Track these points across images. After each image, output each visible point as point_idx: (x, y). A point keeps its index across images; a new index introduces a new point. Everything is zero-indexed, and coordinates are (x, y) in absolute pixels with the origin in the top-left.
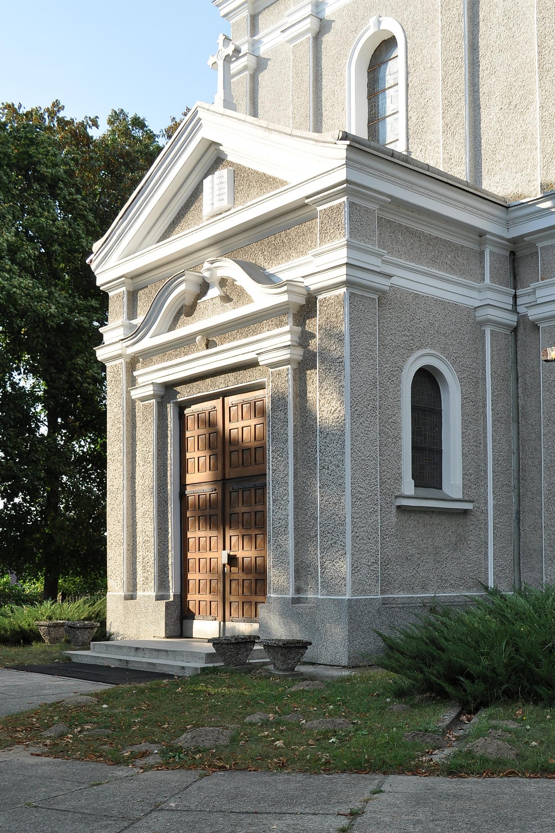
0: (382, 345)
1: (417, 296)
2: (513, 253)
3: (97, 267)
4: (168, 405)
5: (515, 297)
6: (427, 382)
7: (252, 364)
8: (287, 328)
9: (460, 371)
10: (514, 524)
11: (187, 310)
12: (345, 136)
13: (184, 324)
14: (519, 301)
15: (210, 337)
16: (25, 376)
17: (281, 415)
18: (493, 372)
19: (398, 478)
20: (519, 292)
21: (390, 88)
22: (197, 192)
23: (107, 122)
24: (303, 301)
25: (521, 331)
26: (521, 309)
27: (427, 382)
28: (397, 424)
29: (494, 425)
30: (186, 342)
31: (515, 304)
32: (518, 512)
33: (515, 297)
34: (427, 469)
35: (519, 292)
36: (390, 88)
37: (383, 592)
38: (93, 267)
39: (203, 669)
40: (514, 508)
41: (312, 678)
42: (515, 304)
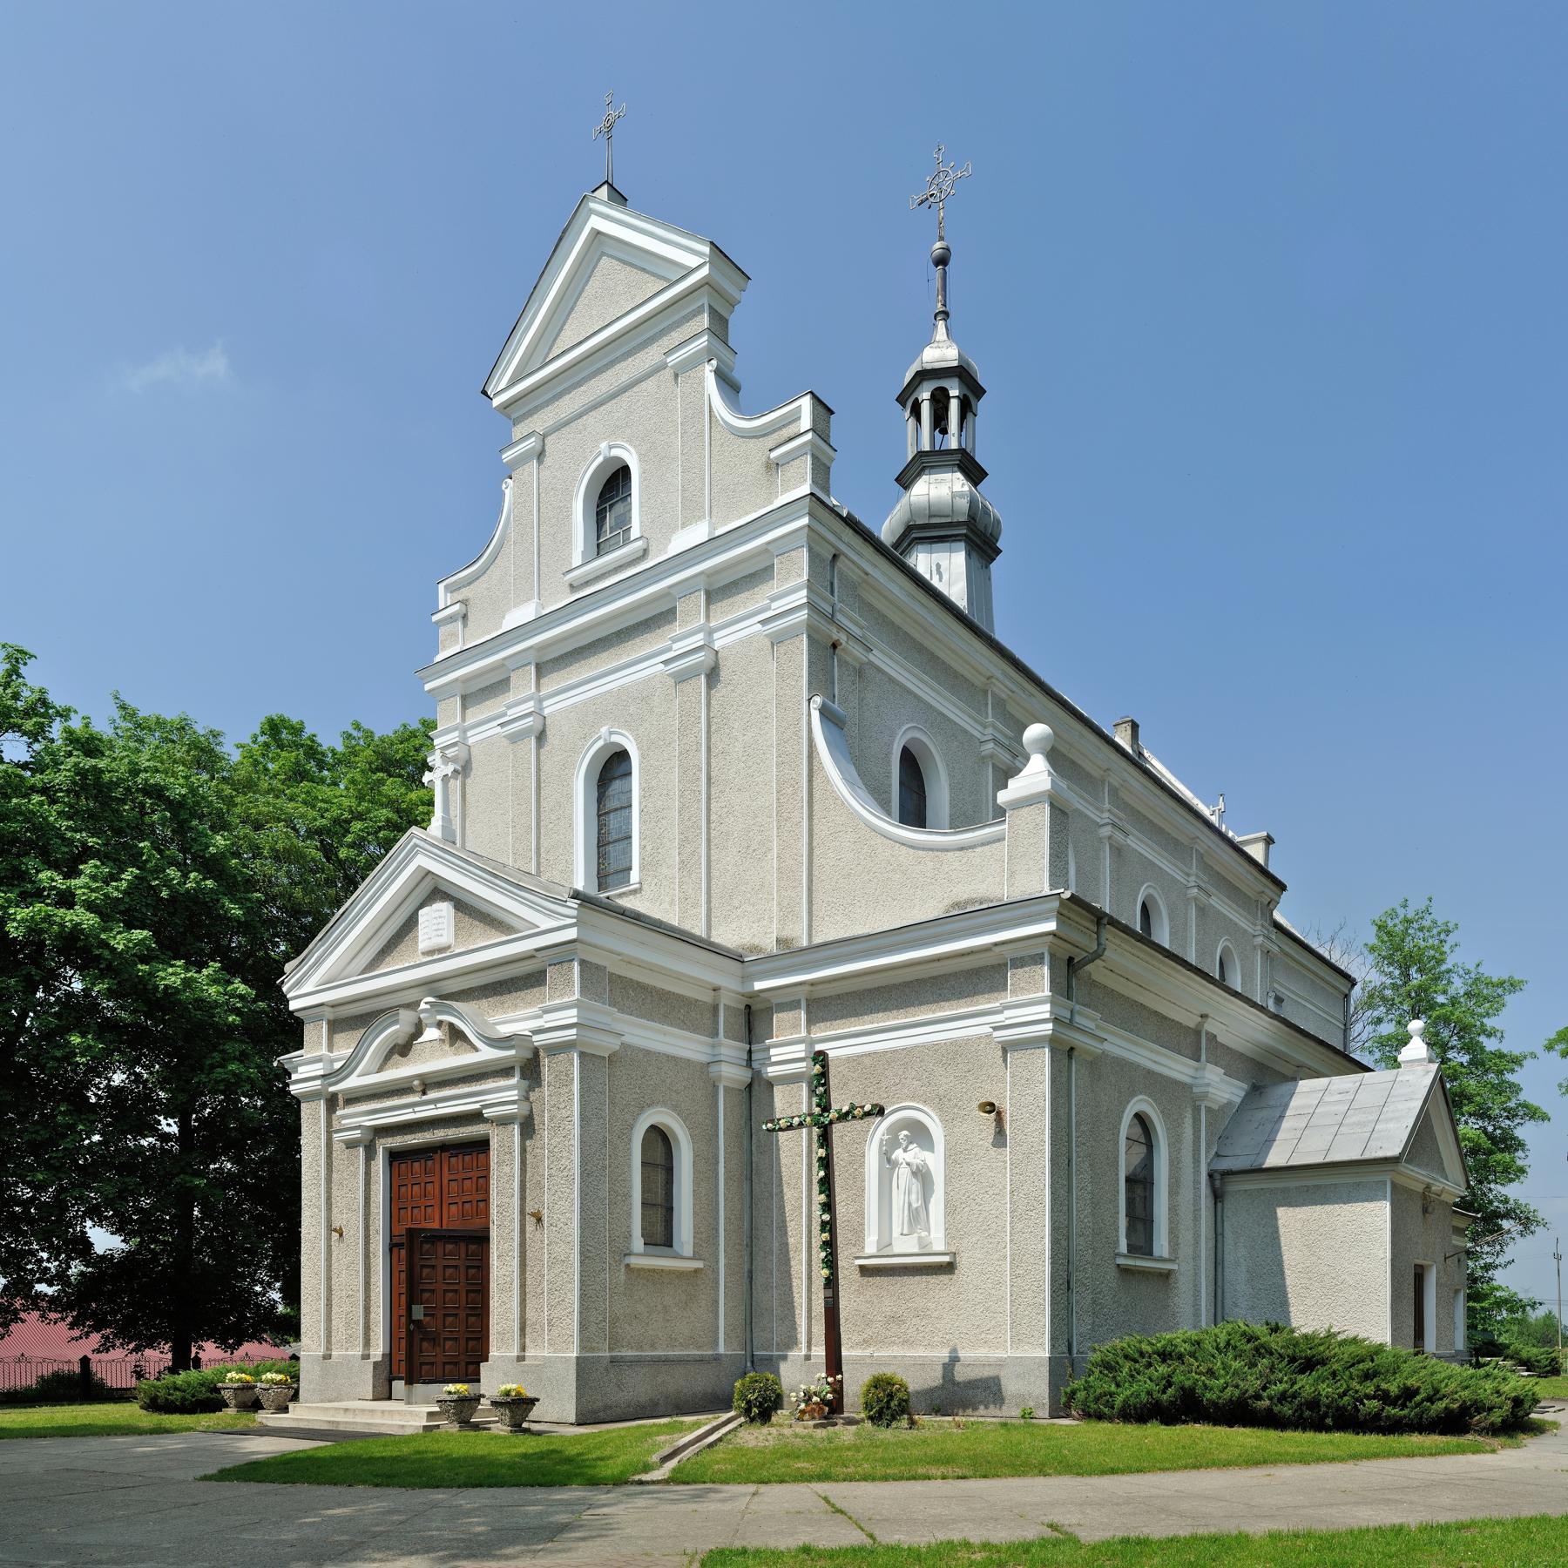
0: (612, 1103)
1: (648, 1053)
2: (748, 1007)
3: (290, 990)
4: (216, 364)
5: (750, 1052)
6: (659, 1138)
7: (476, 1117)
8: (514, 1081)
9: (692, 1128)
10: (746, 1280)
11: (403, 1049)
12: (576, 895)
13: (397, 1065)
14: (754, 1057)
15: (429, 1083)
16: (61, 778)
17: (507, 1169)
18: (727, 1129)
19: (629, 1236)
20: (754, 1047)
21: (617, 872)
22: (411, 923)
23: (274, 713)
24: (529, 1055)
25: (755, 1087)
26: (755, 1065)
27: (659, 1138)
28: (627, 1181)
29: (726, 1183)
30: (399, 1089)
31: (750, 1060)
32: (751, 1271)
33: (750, 1052)
34: (661, 1235)
35: (754, 1047)
36: (617, 872)
37: (611, 1349)
38: (284, 989)
39: (425, 1427)
40: (746, 1267)
41: (539, 1433)
42: (750, 1060)
